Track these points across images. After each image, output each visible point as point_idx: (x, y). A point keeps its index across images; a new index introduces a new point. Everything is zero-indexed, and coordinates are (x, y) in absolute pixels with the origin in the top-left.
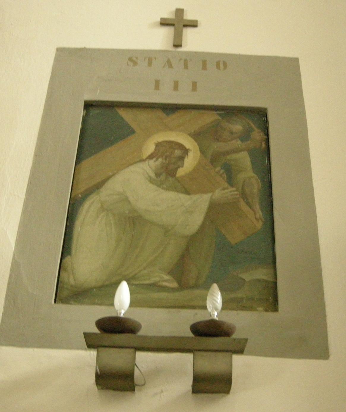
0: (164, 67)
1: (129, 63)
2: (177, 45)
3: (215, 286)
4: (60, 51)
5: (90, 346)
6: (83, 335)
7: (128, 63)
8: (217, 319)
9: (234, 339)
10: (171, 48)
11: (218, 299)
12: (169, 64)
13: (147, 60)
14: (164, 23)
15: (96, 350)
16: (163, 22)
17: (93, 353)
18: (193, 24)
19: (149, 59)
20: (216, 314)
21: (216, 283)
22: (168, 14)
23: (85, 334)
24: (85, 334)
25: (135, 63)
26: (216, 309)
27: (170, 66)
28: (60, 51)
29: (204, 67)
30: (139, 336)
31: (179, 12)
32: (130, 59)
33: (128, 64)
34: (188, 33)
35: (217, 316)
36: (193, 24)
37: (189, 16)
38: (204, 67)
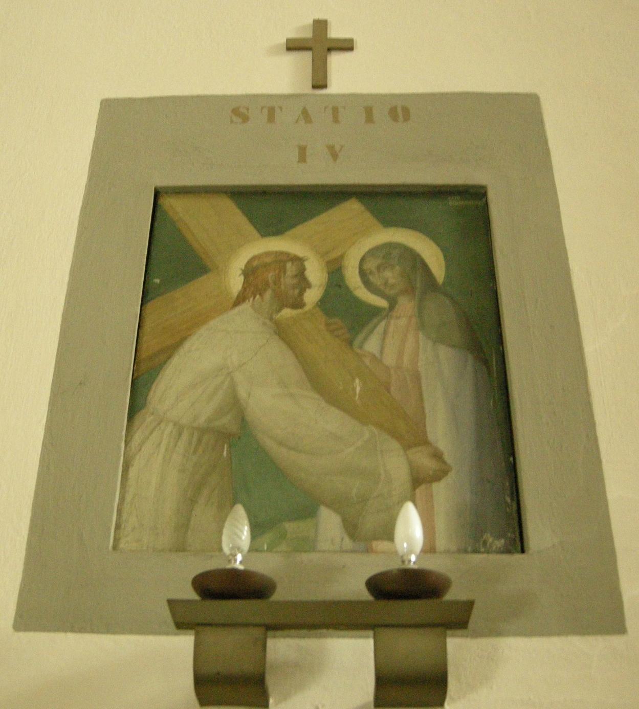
0: (297, 121)
1: (235, 119)
2: (320, 83)
3: (240, 511)
4: (107, 105)
5: (181, 626)
6: (167, 607)
7: (248, 113)
8: (241, 567)
9: (273, 602)
10: (307, 89)
11: (243, 533)
12: (306, 115)
13: (265, 111)
14: (293, 46)
15: (193, 632)
16: (291, 46)
17: (185, 642)
18: (347, 46)
19: (269, 111)
20: (239, 557)
21: (241, 503)
22: (293, 32)
23: (171, 603)
24: (171, 603)
25: (245, 119)
26: (239, 549)
27: (245, 119)
28: (107, 105)
29: (369, 117)
30: (277, 603)
31: (320, 26)
32: (236, 111)
33: (232, 121)
34: (336, 61)
35: (241, 562)
36: (347, 46)
37: (335, 33)
38: (369, 117)
